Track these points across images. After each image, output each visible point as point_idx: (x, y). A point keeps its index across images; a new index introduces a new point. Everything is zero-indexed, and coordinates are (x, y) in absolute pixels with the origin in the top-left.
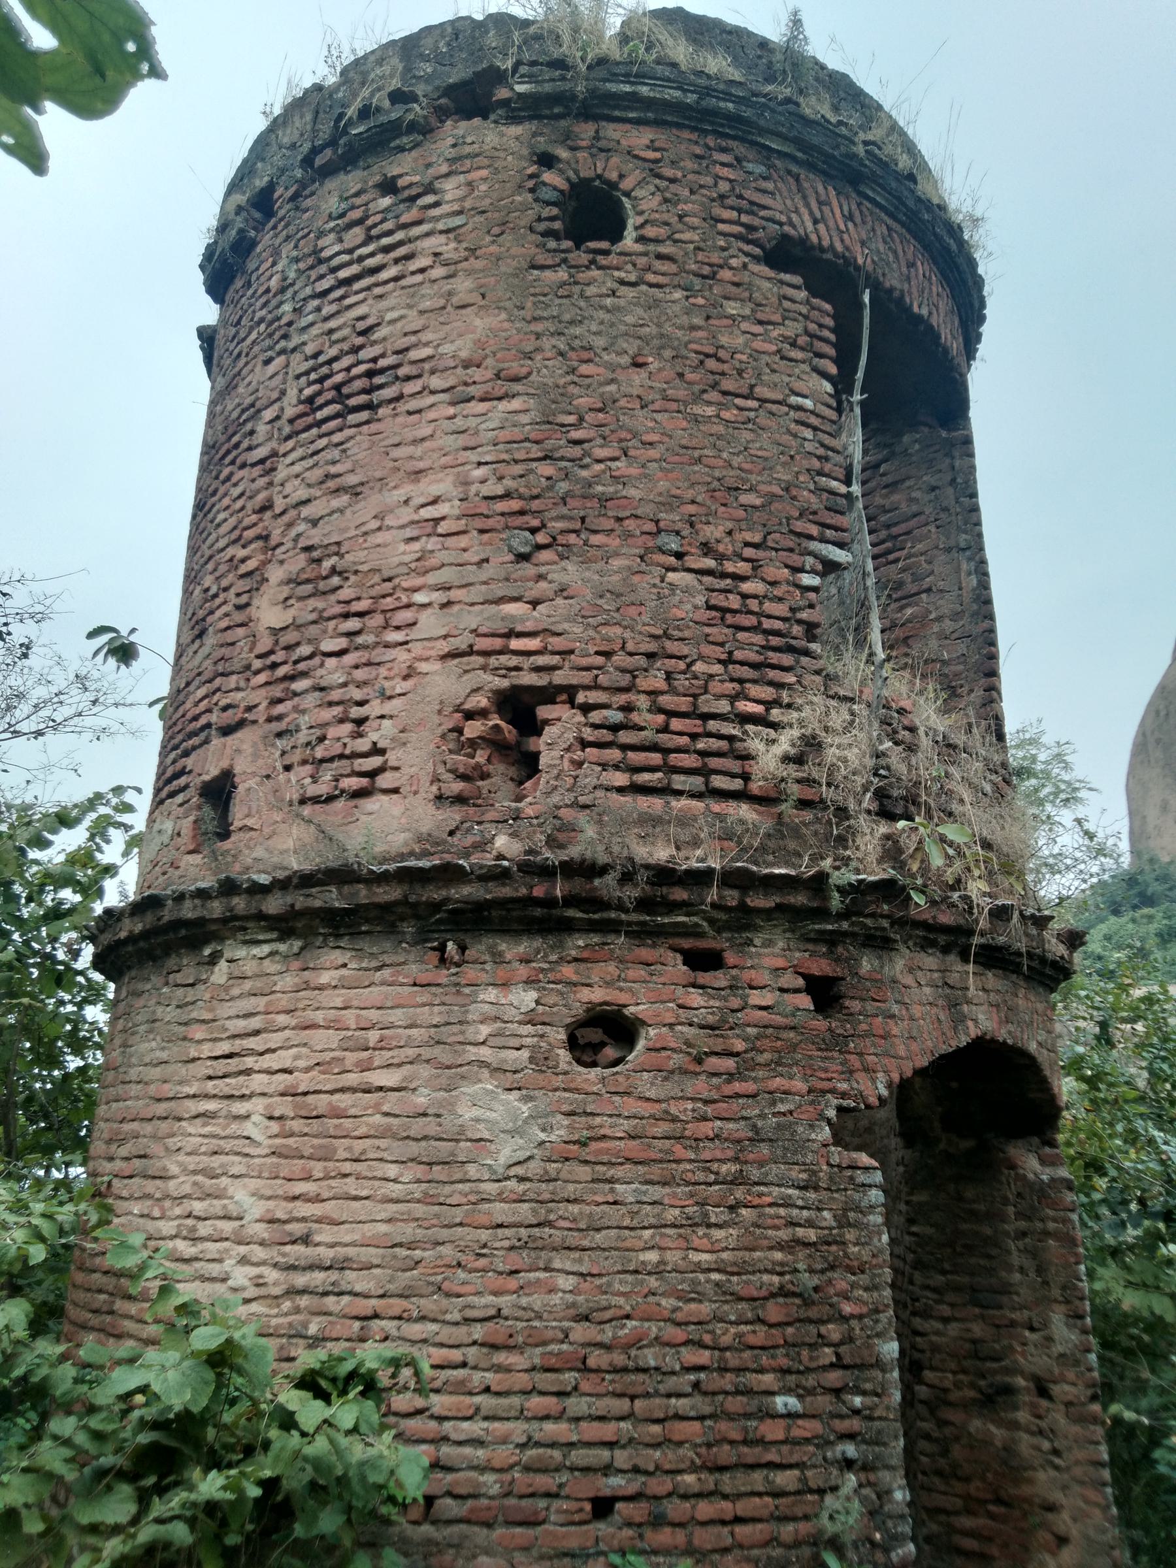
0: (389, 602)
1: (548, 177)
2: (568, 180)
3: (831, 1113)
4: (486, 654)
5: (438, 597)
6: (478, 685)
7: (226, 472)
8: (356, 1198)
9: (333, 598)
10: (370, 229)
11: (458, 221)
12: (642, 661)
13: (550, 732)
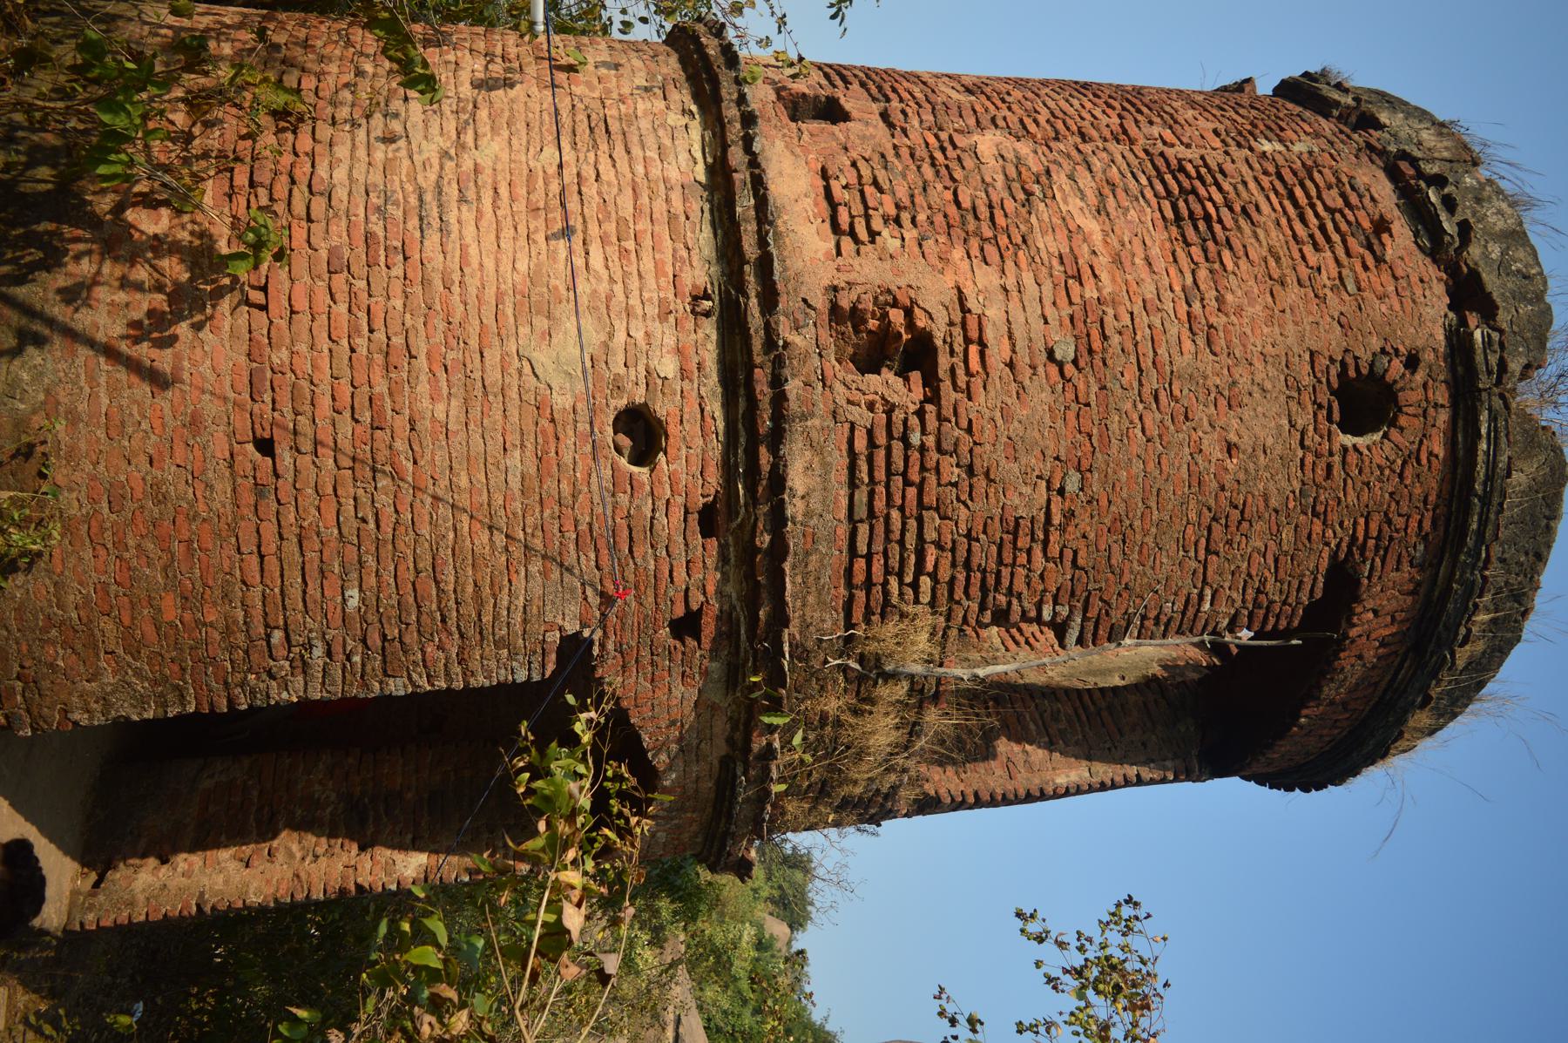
2: (1395, 382)
3: (586, 633)
5: (1011, 282)
7: (1116, 104)
8: (498, 237)
9: (1006, 195)
10: (1341, 211)
11: (1351, 287)
12: (966, 461)
13: (897, 382)
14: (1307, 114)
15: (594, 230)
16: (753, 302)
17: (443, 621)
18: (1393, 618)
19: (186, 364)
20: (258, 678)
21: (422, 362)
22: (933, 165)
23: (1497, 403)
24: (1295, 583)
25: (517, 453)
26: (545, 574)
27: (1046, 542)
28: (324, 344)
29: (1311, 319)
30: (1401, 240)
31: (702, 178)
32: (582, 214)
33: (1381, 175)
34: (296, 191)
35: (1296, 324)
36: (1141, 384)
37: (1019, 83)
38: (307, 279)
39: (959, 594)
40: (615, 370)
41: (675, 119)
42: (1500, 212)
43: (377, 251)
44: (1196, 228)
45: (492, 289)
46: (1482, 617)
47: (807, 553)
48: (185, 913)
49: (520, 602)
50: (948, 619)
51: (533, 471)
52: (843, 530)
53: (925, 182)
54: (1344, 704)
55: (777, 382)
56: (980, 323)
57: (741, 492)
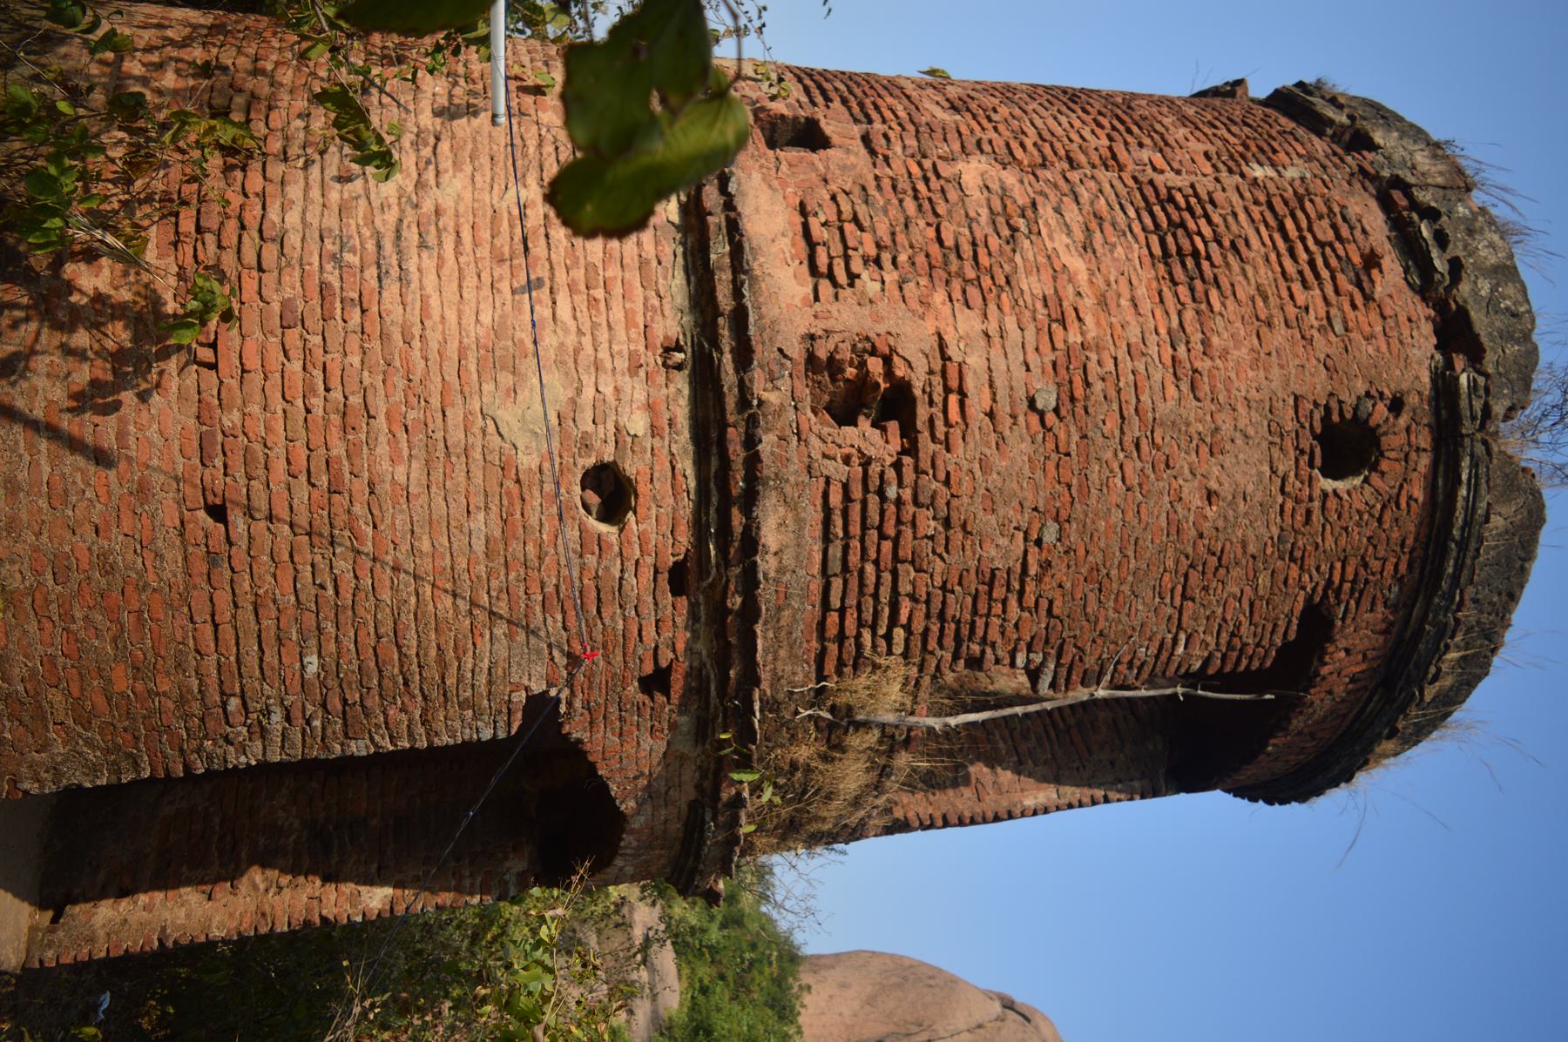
0: (986, 282)
2: (1378, 426)
3: (553, 692)
7: (1105, 122)
8: (460, 287)
9: (989, 230)
10: (1331, 245)
11: (1339, 328)
12: (943, 514)
13: (875, 434)
14: (1301, 132)
15: (561, 277)
16: (727, 358)
17: (406, 684)
18: (1365, 656)
19: (131, 428)
20: (215, 744)
22: (916, 198)
23: (1480, 449)
24: (1269, 627)
25: (481, 516)
26: (510, 636)
27: (1021, 593)
28: (279, 406)
29: (1297, 362)
30: (1391, 276)
32: (549, 259)
33: (1373, 204)
35: (1281, 367)
36: (1122, 432)
37: (1007, 92)
38: (258, 334)
39: (932, 644)
40: (583, 428)
42: (1491, 245)
43: (332, 304)
44: (1184, 265)
45: (450, 345)
46: (1453, 655)
47: (779, 609)
48: (147, 948)
49: (485, 664)
50: (921, 670)
51: (498, 533)
52: (816, 586)
53: (907, 218)
54: (1312, 736)
55: (751, 442)
56: (960, 372)
57: (713, 553)
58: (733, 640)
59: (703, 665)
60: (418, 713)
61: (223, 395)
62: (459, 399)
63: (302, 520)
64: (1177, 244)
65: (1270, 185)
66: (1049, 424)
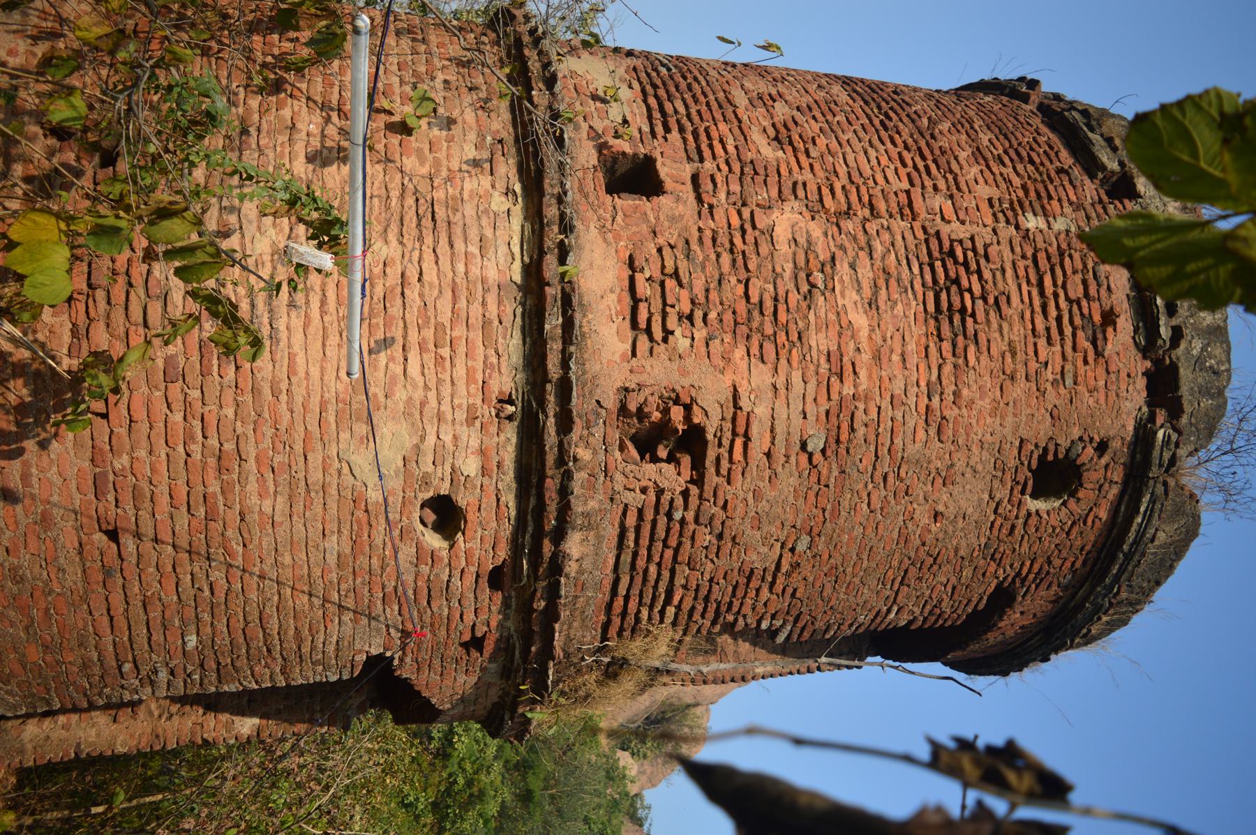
0: (782, 338)
1: (1090, 451)
2: (1084, 464)
3: (388, 654)
4: (734, 420)
5: (781, 383)
6: (712, 421)
7: (907, 156)
8: (324, 345)
9: (791, 286)
10: (1078, 302)
11: (1069, 382)
15: (413, 336)
16: (551, 421)
17: (269, 651)
19: (34, 470)
20: (113, 689)
21: (251, 465)
23: (1160, 489)
24: (965, 602)
25: (335, 538)
26: (355, 621)
27: (772, 584)
28: (162, 451)
29: (1029, 411)
31: (518, 278)
34: (133, 296)
35: (1015, 415)
36: (874, 468)
38: (145, 389)
41: (499, 203)
43: (210, 361)
44: (951, 322)
51: (348, 551)
53: (721, 274)
55: (564, 492)
56: (748, 419)
57: (525, 567)
58: (536, 628)
59: (510, 636)
60: (278, 669)
61: (114, 442)
62: (319, 446)
63: (183, 542)
64: (949, 301)
65: (1039, 239)
66: (815, 462)
